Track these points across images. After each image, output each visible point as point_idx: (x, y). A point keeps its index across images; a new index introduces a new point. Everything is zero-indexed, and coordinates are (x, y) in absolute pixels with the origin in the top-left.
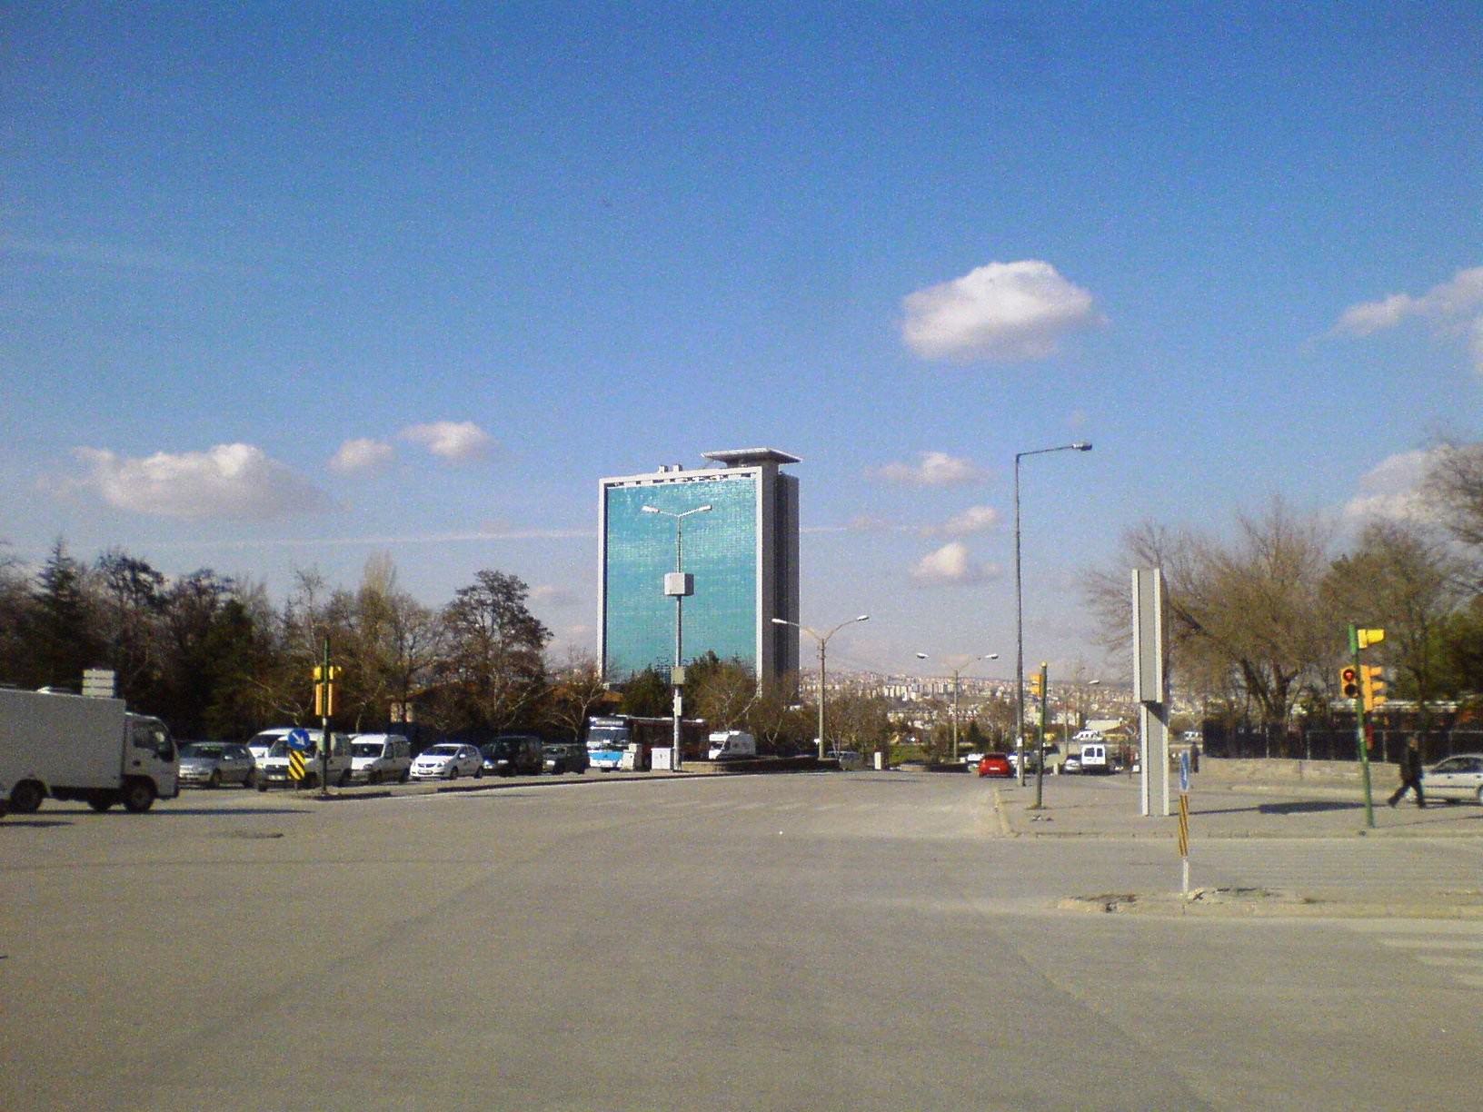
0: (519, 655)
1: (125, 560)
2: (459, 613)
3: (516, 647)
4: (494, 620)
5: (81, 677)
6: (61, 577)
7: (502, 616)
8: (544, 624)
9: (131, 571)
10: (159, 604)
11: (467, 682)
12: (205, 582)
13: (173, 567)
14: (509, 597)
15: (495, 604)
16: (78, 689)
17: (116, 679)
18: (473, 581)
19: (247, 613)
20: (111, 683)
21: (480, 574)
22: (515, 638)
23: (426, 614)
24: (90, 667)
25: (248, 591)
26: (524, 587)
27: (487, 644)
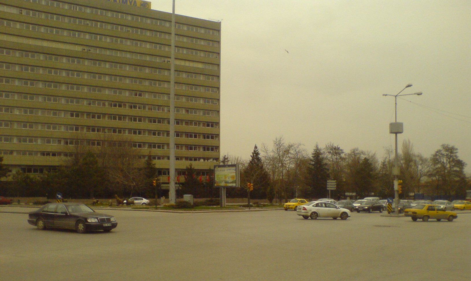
0: (456, 171)
1: (333, 147)
2: (435, 159)
3: (455, 169)
4: (447, 160)
5: (337, 187)
6: (317, 154)
7: (449, 159)
8: (464, 161)
9: (336, 151)
10: (343, 159)
11: (438, 180)
12: (357, 152)
13: (347, 149)
14: (451, 152)
15: (447, 155)
16: (183, 197)
17: (327, 187)
18: (440, 148)
19: (370, 161)
20: (328, 186)
21: (443, 145)
22: (454, 166)
23: (426, 160)
24: (335, 190)
25: (371, 154)
26: (457, 149)
27: (445, 168)
